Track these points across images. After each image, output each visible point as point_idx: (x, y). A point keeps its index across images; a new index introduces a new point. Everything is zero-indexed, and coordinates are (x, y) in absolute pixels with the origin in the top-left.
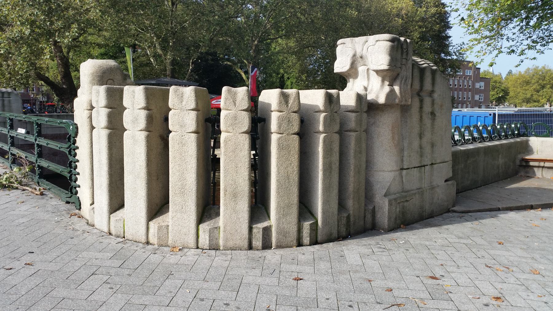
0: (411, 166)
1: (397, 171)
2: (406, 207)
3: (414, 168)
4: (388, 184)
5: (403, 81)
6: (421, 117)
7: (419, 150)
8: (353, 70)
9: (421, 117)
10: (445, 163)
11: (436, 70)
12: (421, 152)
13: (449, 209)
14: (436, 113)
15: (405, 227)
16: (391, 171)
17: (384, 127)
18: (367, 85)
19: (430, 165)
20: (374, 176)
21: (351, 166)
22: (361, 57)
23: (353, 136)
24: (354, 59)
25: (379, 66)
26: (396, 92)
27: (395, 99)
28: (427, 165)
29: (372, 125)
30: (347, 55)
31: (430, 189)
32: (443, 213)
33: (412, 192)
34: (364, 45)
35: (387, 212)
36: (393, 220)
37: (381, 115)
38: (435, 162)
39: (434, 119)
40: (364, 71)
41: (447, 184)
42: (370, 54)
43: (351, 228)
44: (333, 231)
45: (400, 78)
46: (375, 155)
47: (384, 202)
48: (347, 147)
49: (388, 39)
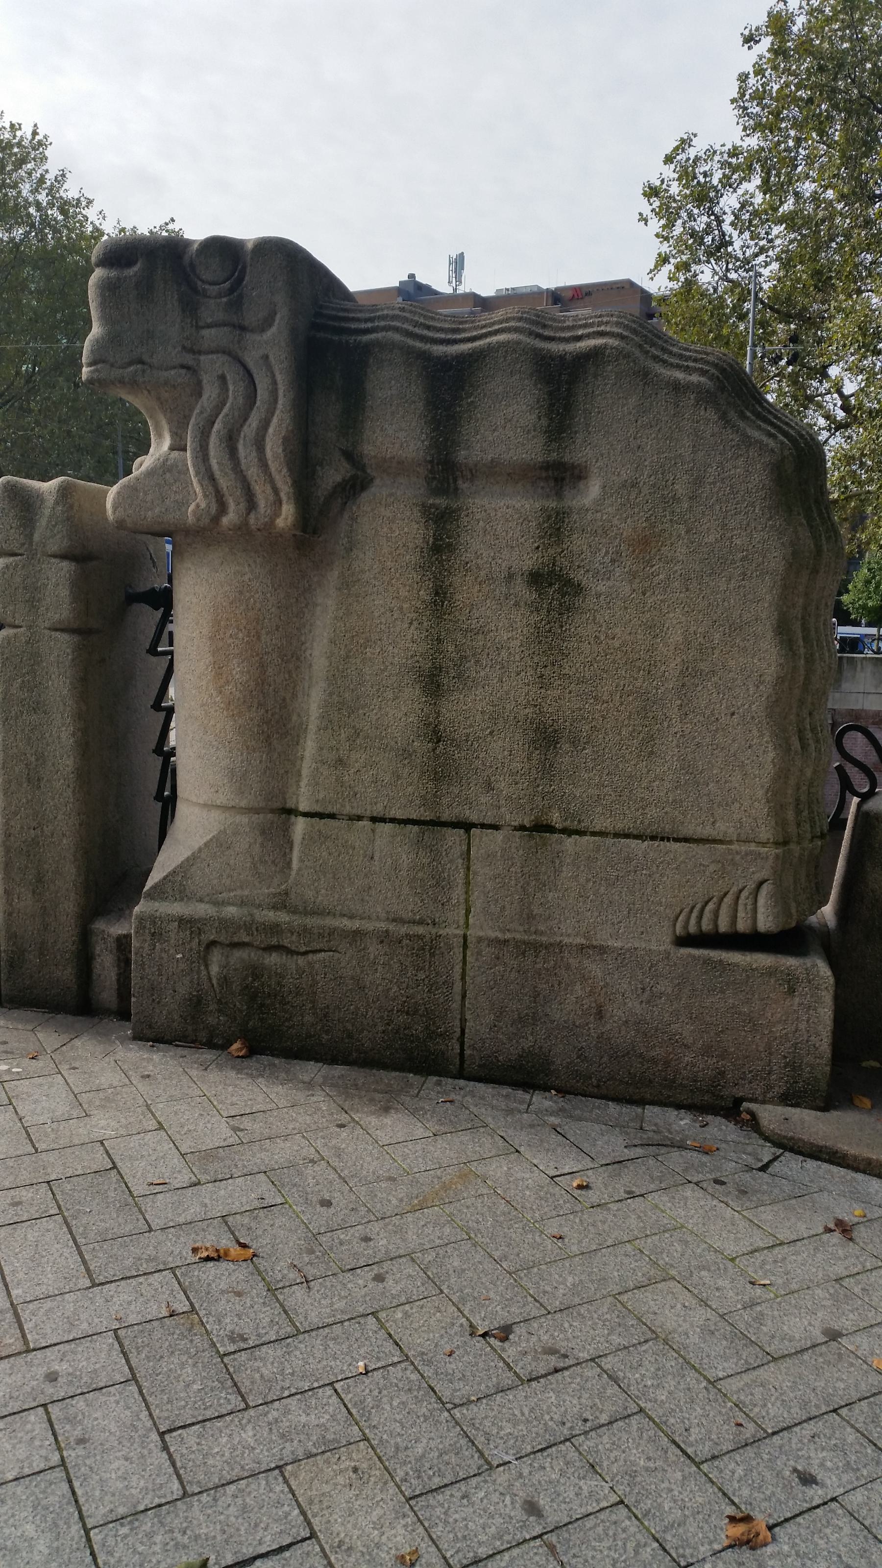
1: (256, 811)
19: (522, 828)
27: (183, 504)
28: (496, 827)
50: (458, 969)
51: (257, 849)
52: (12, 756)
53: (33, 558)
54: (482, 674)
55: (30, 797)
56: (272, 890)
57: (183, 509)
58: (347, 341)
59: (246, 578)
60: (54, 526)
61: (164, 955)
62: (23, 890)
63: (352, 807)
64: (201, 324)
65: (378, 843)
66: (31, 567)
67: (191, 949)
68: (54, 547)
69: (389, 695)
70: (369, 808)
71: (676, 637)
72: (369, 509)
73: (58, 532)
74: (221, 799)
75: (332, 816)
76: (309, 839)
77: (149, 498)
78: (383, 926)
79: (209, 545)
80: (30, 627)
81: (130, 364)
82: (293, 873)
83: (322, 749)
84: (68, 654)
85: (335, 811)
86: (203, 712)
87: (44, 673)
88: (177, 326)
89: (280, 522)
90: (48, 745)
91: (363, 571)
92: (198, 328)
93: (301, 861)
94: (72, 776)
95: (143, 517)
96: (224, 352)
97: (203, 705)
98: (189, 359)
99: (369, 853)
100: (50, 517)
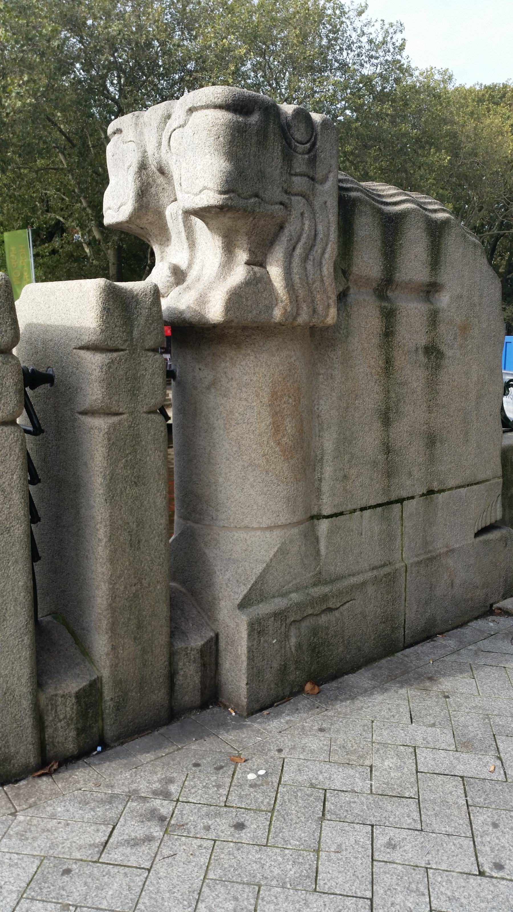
0: (350, 507)
1: (300, 523)
2: (328, 628)
3: (362, 509)
4: (259, 569)
5: (299, 251)
6: (388, 362)
7: (381, 457)
8: (151, 217)
9: (388, 362)
10: (475, 487)
11: (446, 223)
12: (387, 462)
13: (491, 605)
14: (443, 348)
15: (316, 690)
16: (270, 528)
17: (244, 395)
18: (187, 263)
19: (423, 495)
20: (218, 542)
21: (98, 527)
22: (162, 171)
23: (100, 430)
24: (144, 177)
25: (196, 195)
26: (276, 284)
27: (270, 308)
28: (412, 498)
29: (208, 388)
30: (126, 168)
31: (419, 563)
32: (469, 621)
33: (353, 580)
34: (163, 130)
35: (244, 658)
36: (269, 676)
37: (232, 359)
38: (441, 487)
39: (438, 367)
40: (176, 218)
41: (486, 543)
42: (174, 157)
43: (108, 721)
44: (13, 749)
45: (284, 238)
46: (221, 480)
47: (238, 625)
48: (86, 464)
49: (219, 101)
50: (404, 586)
51: (303, 548)
52: (118, 528)
53: (134, 353)
54: (406, 409)
55: (132, 559)
56: (312, 574)
57: (270, 312)
58: (344, 195)
59: (292, 360)
60: (151, 324)
61: (266, 645)
62: (126, 641)
63: (351, 505)
64: (293, 172)
65: (364, 523)
66: (132, 362)
67: (281, 633)
68: (150, 342)
69: (367, 429)
70: (359, 502)
71: (475, 379)
72: (356, 309)
73: (154, 330)
74: (282, 520)
75: (341, 514)
76: (331, 533)
77: (249, 303)
78: (369, 575)
79: (268, 337)
80: (132, 413)
81: (251, 197)
82: (323, 558)
83: (336, 471)
84: (162, 432)
85: (343, 510)
86: (265, 461)
87: (143, 450)
88: (278, 171)
89: (300, 320)
90: (146, 511)
91: (353, 351)
92: (291, 175)
93: (327, 548)
94: (164, 531)
95: (245, 318)
96: (301, 195)
97: (264, 455)
98: (285, 198)
99: (360, 531)
100: (148, 316)
